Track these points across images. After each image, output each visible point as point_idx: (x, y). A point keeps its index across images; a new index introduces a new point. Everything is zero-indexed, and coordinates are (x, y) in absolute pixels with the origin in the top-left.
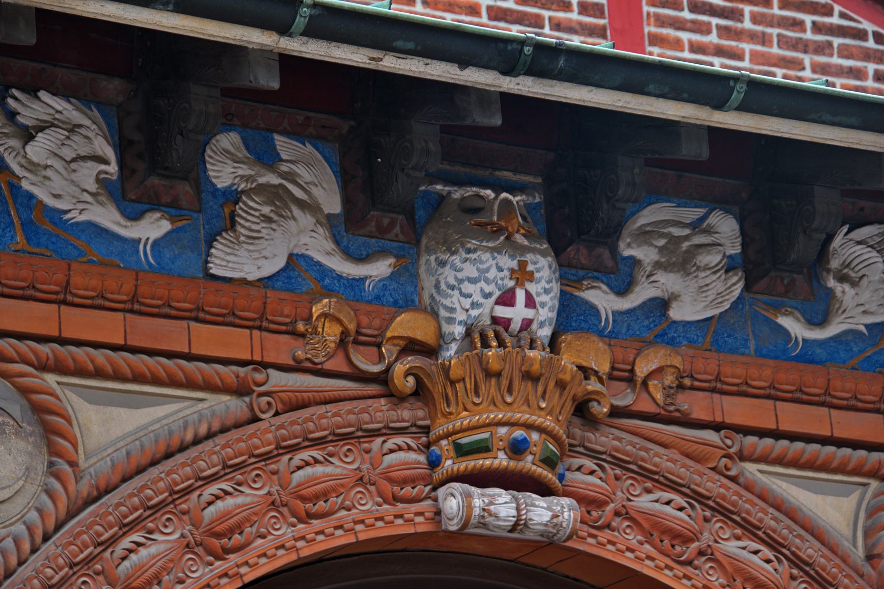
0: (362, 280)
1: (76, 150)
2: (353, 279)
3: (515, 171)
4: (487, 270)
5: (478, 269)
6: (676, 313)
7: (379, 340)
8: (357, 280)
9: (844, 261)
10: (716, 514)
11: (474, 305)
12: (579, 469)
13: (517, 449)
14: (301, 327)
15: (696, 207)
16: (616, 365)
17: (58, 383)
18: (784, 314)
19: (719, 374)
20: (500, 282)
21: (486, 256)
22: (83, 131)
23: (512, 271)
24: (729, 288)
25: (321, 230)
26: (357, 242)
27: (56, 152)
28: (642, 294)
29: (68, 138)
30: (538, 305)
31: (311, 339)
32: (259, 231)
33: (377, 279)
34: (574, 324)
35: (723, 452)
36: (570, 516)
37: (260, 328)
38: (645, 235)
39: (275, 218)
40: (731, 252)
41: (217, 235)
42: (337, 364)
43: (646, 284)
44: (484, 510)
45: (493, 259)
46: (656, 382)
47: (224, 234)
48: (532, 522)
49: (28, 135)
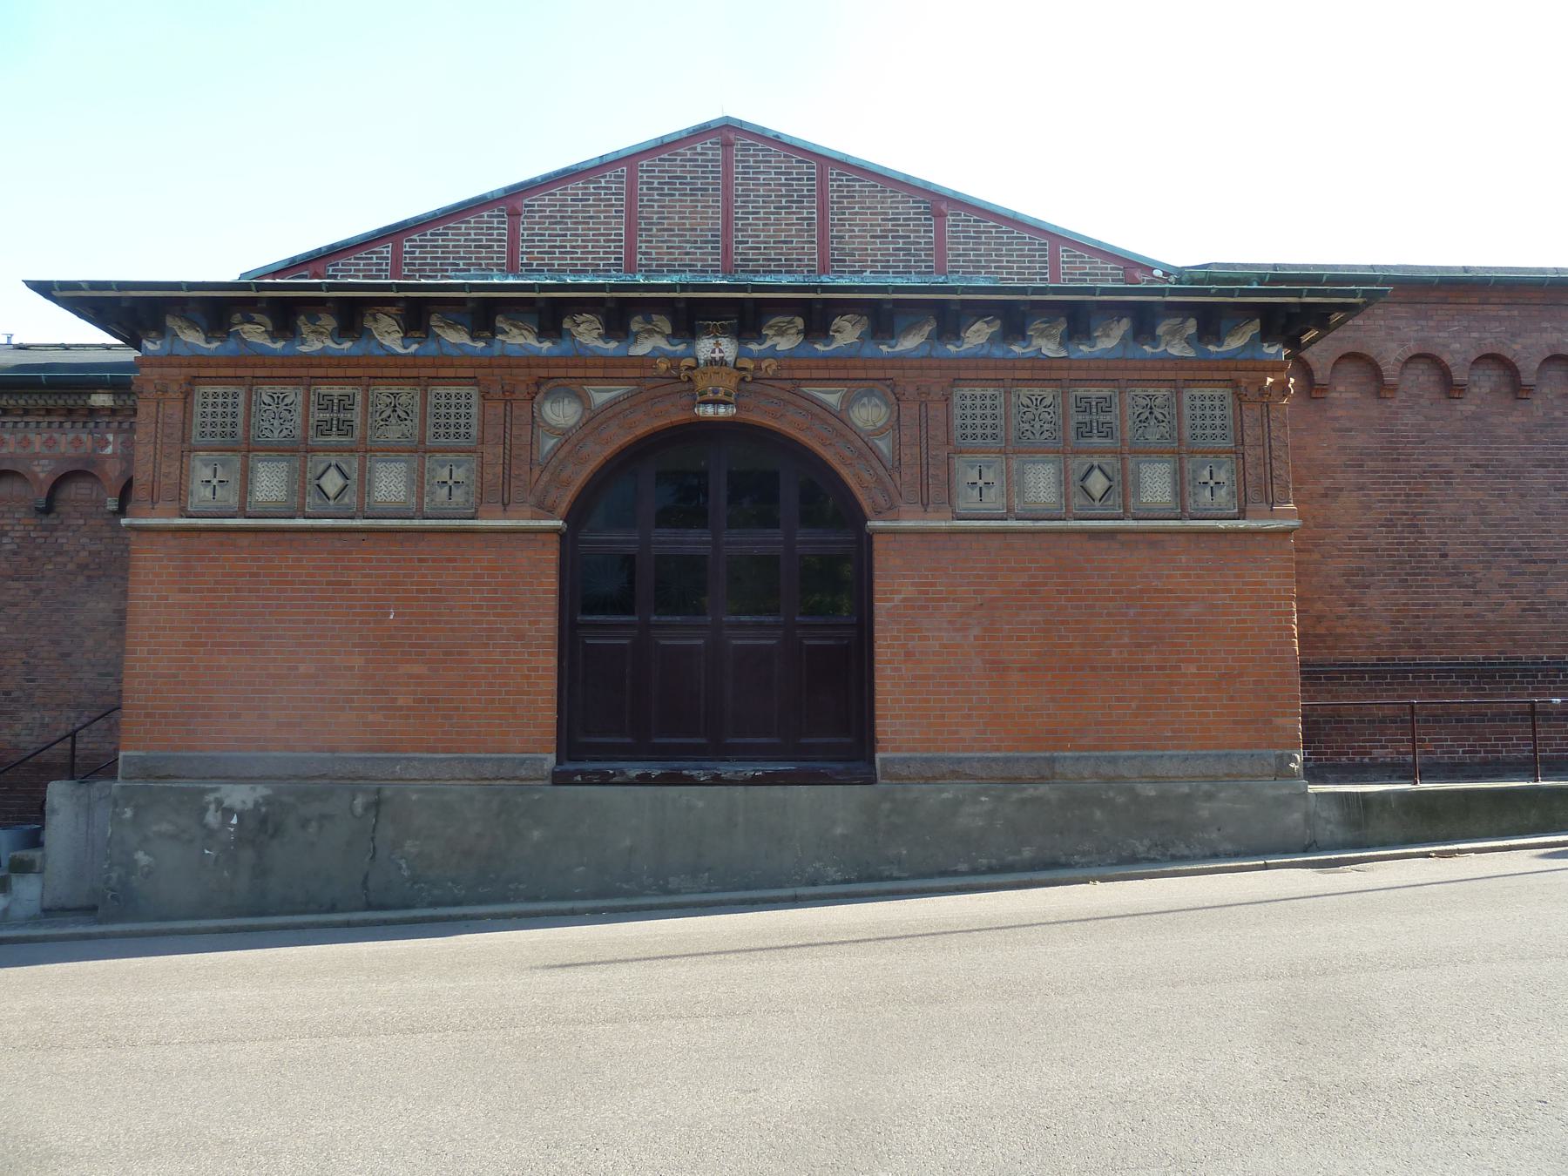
6: (778, 348)
26: (676, 341)
38: (771, 327)
42: (667, 375)
49: (579, 325)
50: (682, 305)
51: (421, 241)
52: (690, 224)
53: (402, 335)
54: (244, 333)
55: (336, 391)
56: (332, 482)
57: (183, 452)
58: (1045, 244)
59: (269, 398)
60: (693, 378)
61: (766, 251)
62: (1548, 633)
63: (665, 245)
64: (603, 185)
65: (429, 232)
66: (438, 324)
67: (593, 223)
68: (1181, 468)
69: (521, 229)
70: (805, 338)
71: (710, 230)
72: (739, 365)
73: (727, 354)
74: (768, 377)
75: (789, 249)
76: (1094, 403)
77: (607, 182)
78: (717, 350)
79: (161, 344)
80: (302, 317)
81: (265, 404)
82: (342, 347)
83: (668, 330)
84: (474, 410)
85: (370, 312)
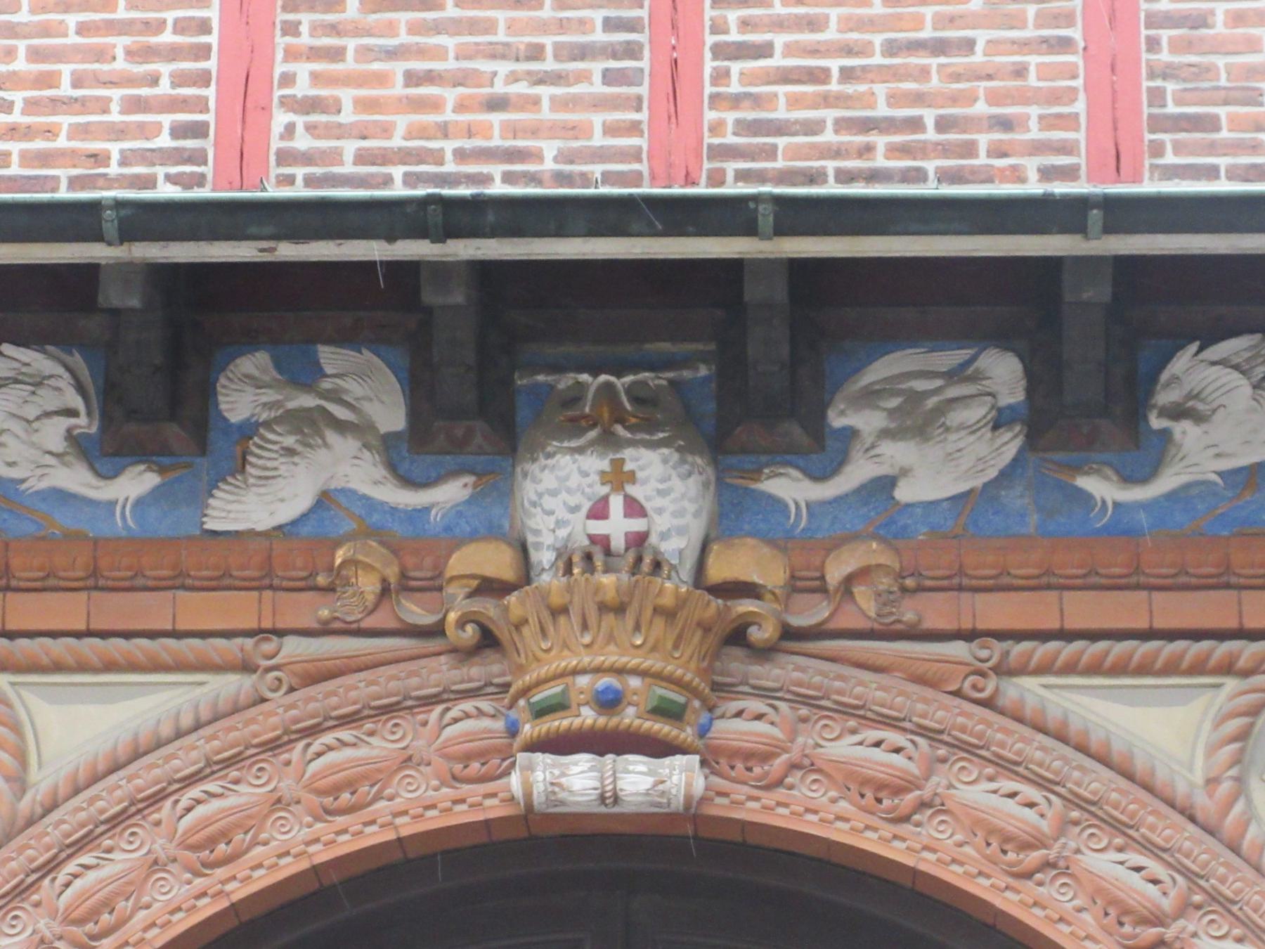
0: (426, 510)
1: (41, 406)
2: (415, 510)
3: (672, 339)
4: (567, 478)
5: (558, 478)
6: (905, 493)
7: (437, 583)
8: (419, 511)
9: (1192, 390)
10: (956, 750)
11: (560, 523)
12: (739, 714)
13: (609, 702)
14: (321, 580)
15: (959, 348)
16: (798, 574)
17: (13, 684)
18: (1087, 473)
19: (961, 566)
20: (587, 490)
21: (567, 459)
22: (52, 382)
23: (603, 473)
24: (997, 449)
25: (367, 454)
27: (15, 412)
28: (857, 473)
29: (33, 393)
30: (650, 512)
31: (344, 593)
32: (276, 469)
33: (448, 506)
34: (746, 527)
35: (968, 669)
36: (681, 779)
37: (271, 587)
38: (870, 397)
39: (299, 448)
40: (1006, 400)
41: (217, 481)
42: (379, 620)
43: (862, 461)
44: (552, 784)
45: (574, 463)
46: (863, 588)
47: (230, 480)
48: (623, 793)
50: (1099, 292)
60: (503, 633)
61: (850, 89)
70: (1033, 440)
72: (718, 571)
73: (661, 523)
75: (957, 77)
78: (617, 503)
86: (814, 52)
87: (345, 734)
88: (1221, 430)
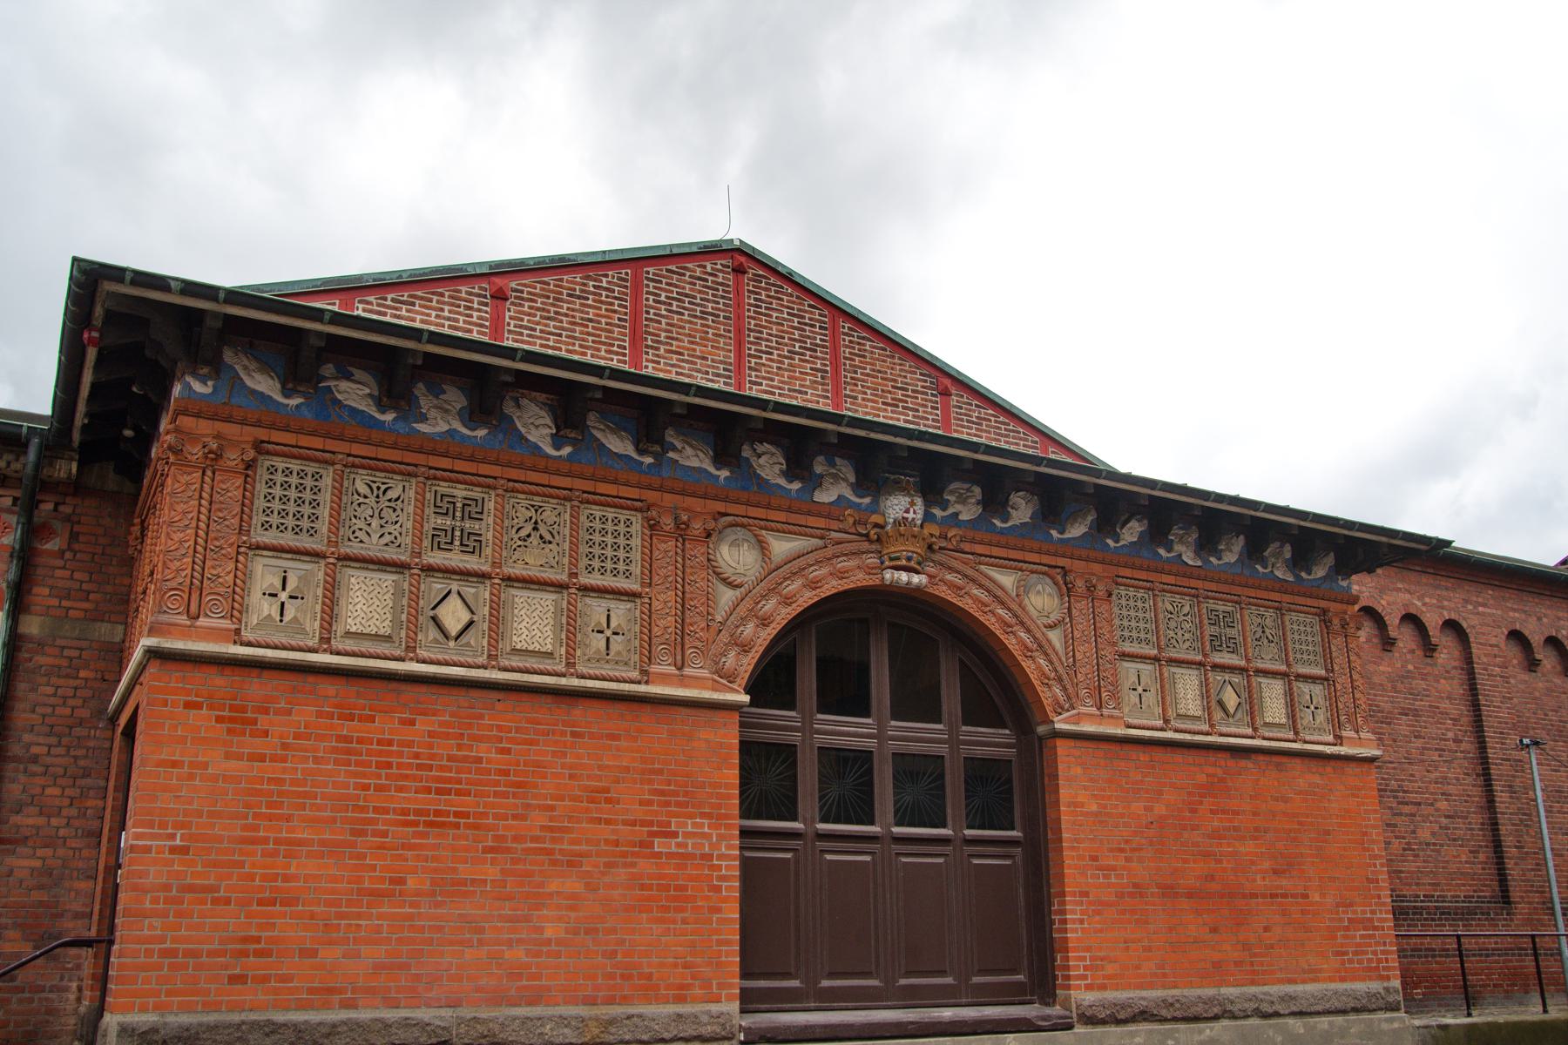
6: (961, 517)
13: (909, 559)
28: (950, 511)
38: (952, 492)
42: (853, 530)
49: (759, 456)
51: (378, 305)
52: (701, 352)
53: (554, 431)
54: (340, 393)
55: (460, 492)
56: (453, 615)
57: (239, 547)
58: (1036, 442)
59: (365, 486)
62: (1421, 872)
63: (674, 370)
64: (604, 285)
65: (390, 297)
66: (597, 425)
67: (593, 328)
68: (1290, 689)
69: (507, 317)
71: (721, 362)
74: (952, 547)
76: (459, 505)
77: (608, 282)
79: (214, 386)
80: (421, 385)
81: (359, 495)
82: (474, 434)
83: (852, 479)
84: (636, 542)
85: (511, 394)
86: (772, 387)
87: (845, 558)
88: (1020, 513)
